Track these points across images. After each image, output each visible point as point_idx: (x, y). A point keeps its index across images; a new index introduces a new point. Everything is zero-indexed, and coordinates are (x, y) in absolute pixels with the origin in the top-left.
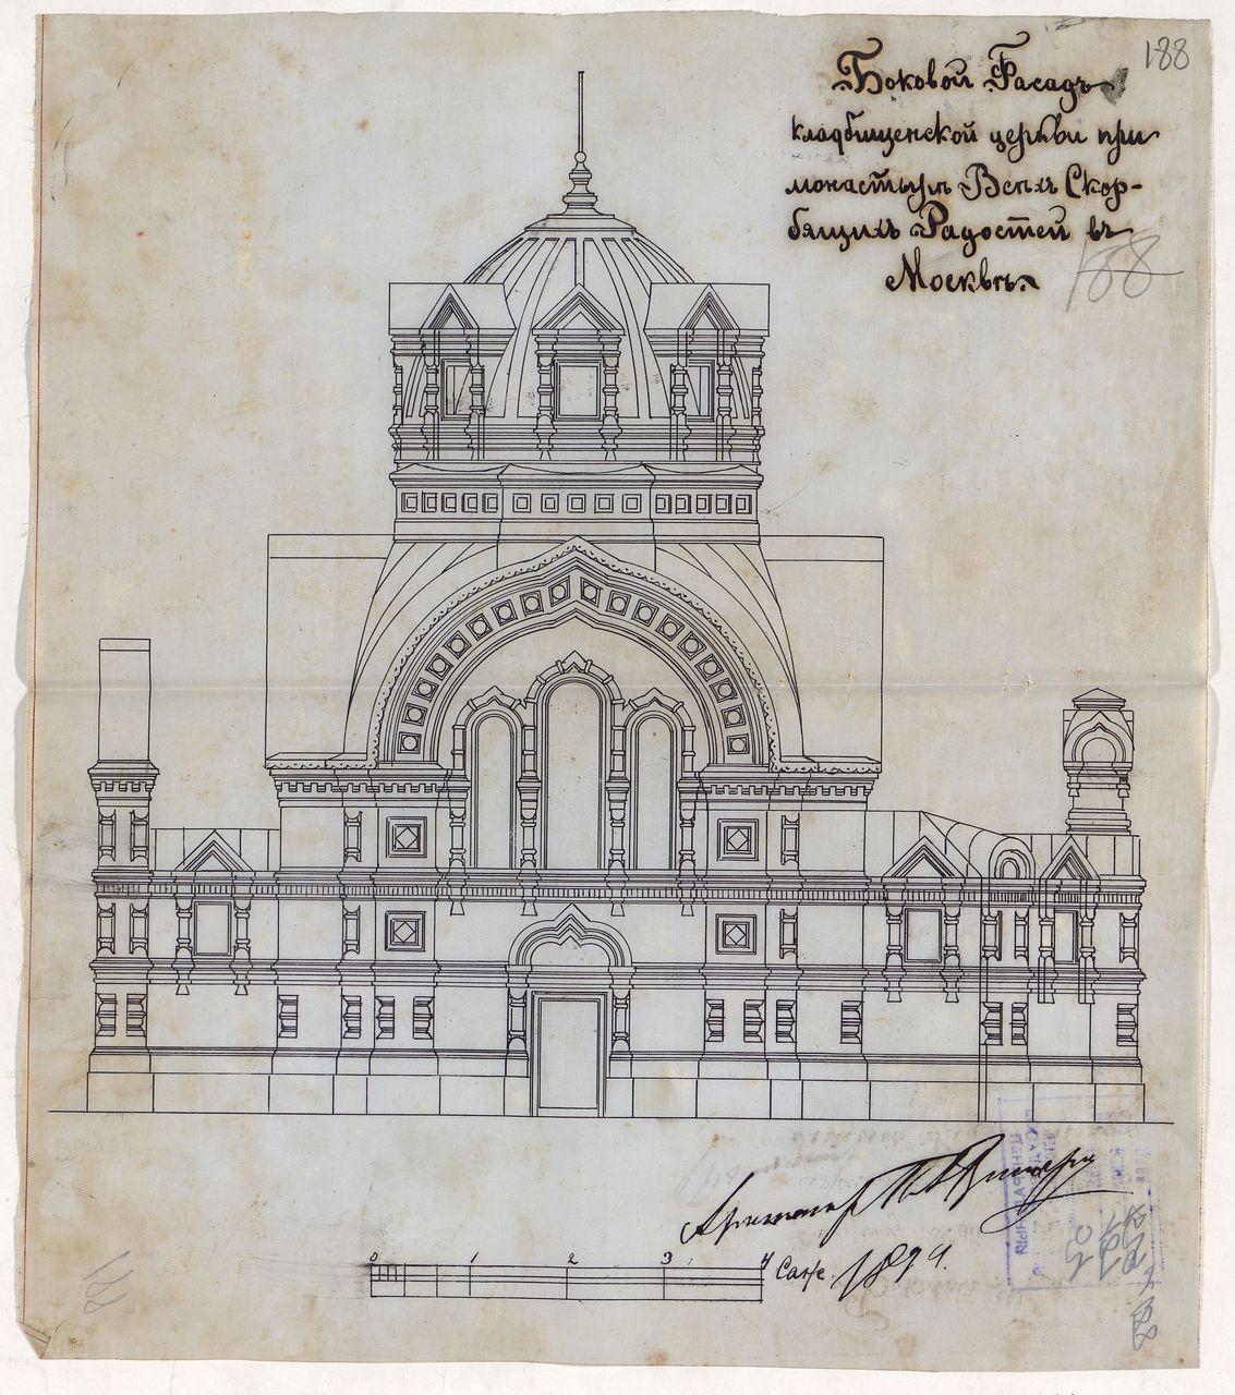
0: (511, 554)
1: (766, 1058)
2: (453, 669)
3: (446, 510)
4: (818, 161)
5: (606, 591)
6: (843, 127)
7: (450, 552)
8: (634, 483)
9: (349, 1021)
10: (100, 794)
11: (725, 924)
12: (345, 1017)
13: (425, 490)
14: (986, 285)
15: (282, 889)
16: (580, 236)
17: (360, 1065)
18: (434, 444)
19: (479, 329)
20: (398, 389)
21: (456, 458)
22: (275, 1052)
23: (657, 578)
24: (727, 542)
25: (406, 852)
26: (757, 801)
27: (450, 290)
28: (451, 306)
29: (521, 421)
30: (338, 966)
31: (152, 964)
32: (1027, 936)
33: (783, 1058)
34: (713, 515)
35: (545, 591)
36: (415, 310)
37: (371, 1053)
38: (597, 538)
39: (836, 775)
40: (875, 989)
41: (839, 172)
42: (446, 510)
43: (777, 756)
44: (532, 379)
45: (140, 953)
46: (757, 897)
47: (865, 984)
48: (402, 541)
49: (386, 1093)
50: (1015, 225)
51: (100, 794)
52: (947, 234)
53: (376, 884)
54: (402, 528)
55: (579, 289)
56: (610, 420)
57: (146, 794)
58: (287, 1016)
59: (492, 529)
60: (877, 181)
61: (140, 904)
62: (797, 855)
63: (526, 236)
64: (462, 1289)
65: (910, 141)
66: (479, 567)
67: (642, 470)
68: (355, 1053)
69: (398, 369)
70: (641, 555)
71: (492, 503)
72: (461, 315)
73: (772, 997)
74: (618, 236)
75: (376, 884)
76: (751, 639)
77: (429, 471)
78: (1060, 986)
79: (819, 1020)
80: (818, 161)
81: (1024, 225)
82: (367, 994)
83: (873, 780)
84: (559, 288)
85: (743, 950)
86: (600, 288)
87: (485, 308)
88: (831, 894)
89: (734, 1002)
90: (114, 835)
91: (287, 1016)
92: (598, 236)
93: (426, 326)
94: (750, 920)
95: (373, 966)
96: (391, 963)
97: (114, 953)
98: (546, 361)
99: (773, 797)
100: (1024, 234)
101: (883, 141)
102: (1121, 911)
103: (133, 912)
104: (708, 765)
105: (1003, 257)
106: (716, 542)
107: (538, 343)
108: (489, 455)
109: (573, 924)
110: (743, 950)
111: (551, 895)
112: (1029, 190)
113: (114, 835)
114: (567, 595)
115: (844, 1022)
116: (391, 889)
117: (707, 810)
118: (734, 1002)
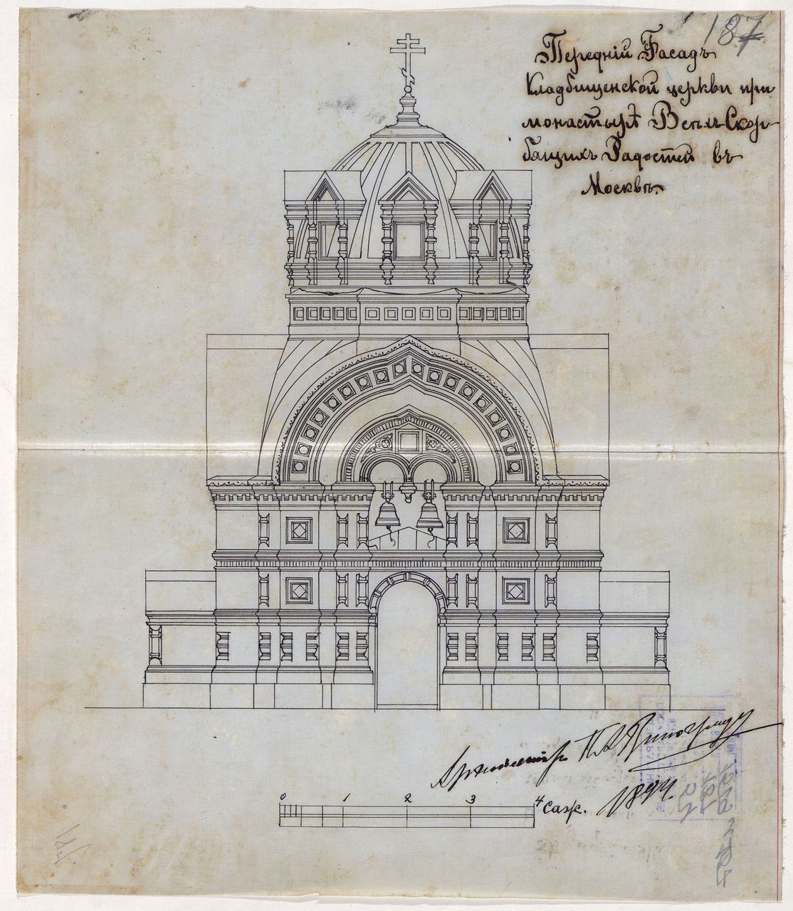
0: (363, 346)
1: (536, 670)
2: (329, 419)
3: (297, 319)
4: (544, 107)
5: (427, 368)
6: (565, 85)
7: (328, 345)
8: (449, 300)
9: (263, 652)
10: (448, 503)
11: (523, 584)
12: (338, 646)
13: (440, 305)
14: (637, 190)
15: (261, 563)
16: (409, 141)
17: (271, 677)
18: (345, 275)
19: (512, 200)
20: (290, 240)
21: (328, 282)
22: (214, 669)
23: (460, 360)
24: (509, 339)
25: (517, 540)
26: (352, 506)
27: (325, 176)
28: (324, 187)
29: (372, 261)
30: (257, 613)
31: (480, 614)
32: (346, 589)
33: (547, 670)
34: (485, 321)
35: (390, 368)
36: (302, 189)
37: (278, 670)
38: (480, 336)
39: (551, 488)
40: (486, 626)
41: (564, 113)
42: (297, 319)
43: (540, 475)
44: (378, 233)
45: (472, 607)
46: (362, 565)
47: (537, 622)
48: (294, 339)
49: (286, 695)
50: (666, 154)
51: (448, 503)
52: (625, 158)
53: (536, 560)
54: (293, 330)
55: (409, 175)
56: (431, 261)
57: (368, 503)
58: (222, 646)
59: (354, 330)
60: (588, 120)
61: (552, 575)
62: (477, 540)
63: (373, 141)
64: (318, 822)
65: (613, 92)
66: (347, 353)
67: (453, 291)
68: (267, 669)
69: (290, 226)
70: (452, 346)
71: (353, 314)
72: (333, 194)
73: (540, 632)
74: (434, 141)
75: (536, 560)
76: (524, 402)
77: (304, 293)
78: (605, 622)
79: (572, 645)
80: (544, 107)
81: (671, 153)
82: (275, 632)
83: (604, 490)
84: (394, 175)
85: (521, 601)
86: (422, 174)
87: (346, 186)
88: (456, 563)
89: (515, 635)
90: (347, 531)
91: (222, 646)
92: (422, 140)
93: (310, 199)
94: (526, 582)
95: (279, 613)
96: (288, 611)
97: (268, 606)
98: (387, 222)
99: (323, 503)
100: (669, 160)
101: (596, 91)
102: (546, 573)
103: (548, 580)
104: (496, 482)
105: (653, 173)
106: (484, 339)
107: (383, 210)
108: (352, 283)
109: (293, 581)
110: (521, 601)
111: (459, 565)
112: (699, 127)
113: (347, 531)
114: (405, 371)
115: (588, 647)
116: (431, 563)
117: (557, 510)
118: (515, 635)
